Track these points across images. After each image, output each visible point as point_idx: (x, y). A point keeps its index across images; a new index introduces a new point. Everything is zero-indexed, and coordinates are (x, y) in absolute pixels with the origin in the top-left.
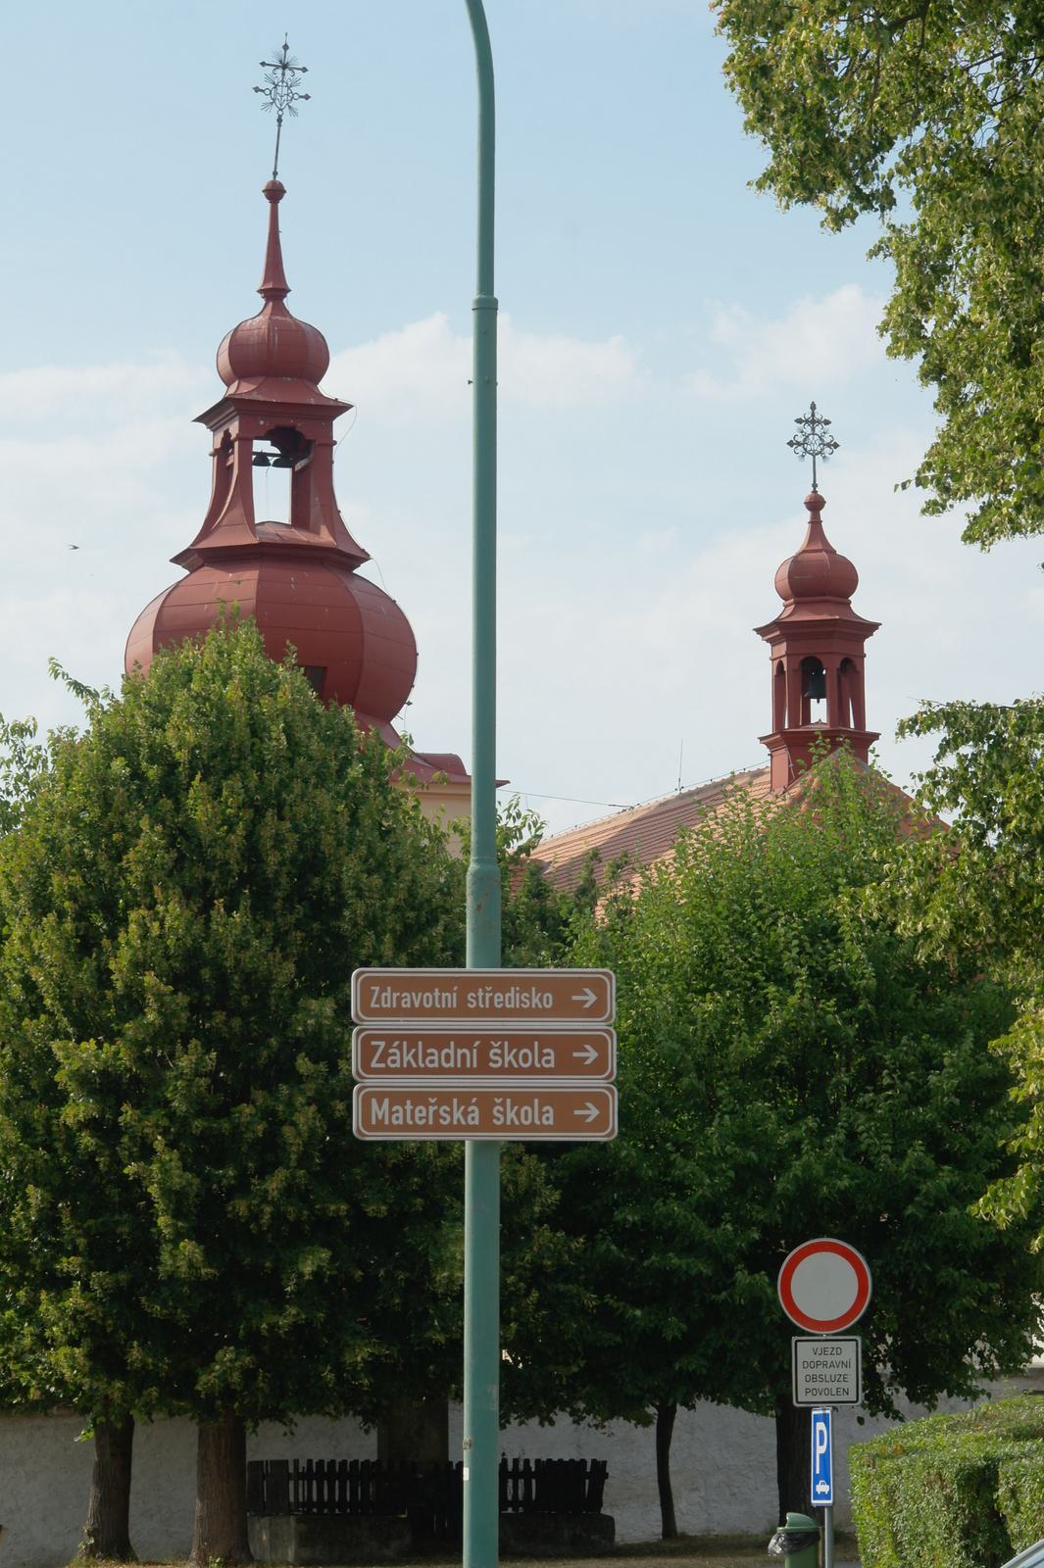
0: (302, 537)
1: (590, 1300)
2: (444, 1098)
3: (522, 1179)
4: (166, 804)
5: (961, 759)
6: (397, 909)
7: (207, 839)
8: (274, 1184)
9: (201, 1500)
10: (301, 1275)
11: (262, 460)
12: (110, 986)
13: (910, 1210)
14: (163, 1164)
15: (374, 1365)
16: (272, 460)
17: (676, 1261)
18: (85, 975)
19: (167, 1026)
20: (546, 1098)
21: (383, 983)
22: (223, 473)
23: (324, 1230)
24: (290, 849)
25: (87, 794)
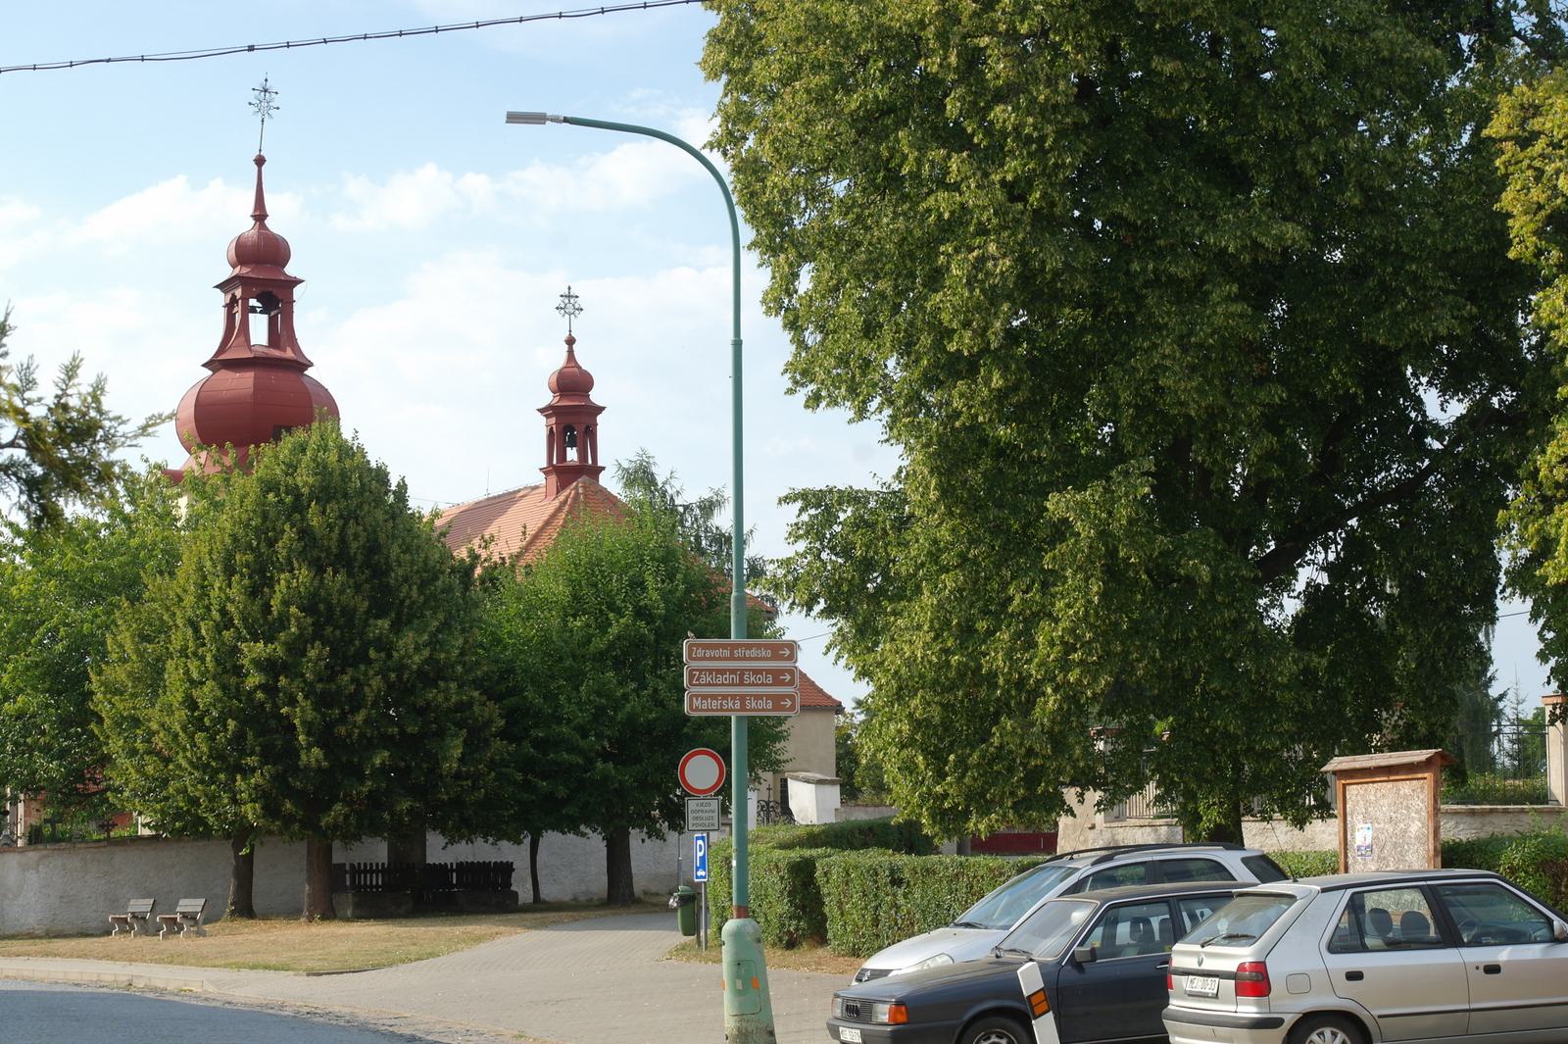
0: (277, 353)
1: (519, 777)
2: (725, 697)
3: (487, 715)
4: (297, 516)
5: (810, 516)
6: (418, 572)
7: (319, 536)
8: (360, 718)
9: (309, 884)
10: (373, 765)
11: (253, 310)
12: (270, 613)
13: (686, 730)
14: (302, 707)
15: (411, 811)
16: (258, 310)
17: (565, 756)
18: (256, 608)
19: (301, 635)
20: (768, 697)
21: (698, 646)
22: (230, 317)
23: (386, 741)
24: (362, 540)
25: (254, 511)
